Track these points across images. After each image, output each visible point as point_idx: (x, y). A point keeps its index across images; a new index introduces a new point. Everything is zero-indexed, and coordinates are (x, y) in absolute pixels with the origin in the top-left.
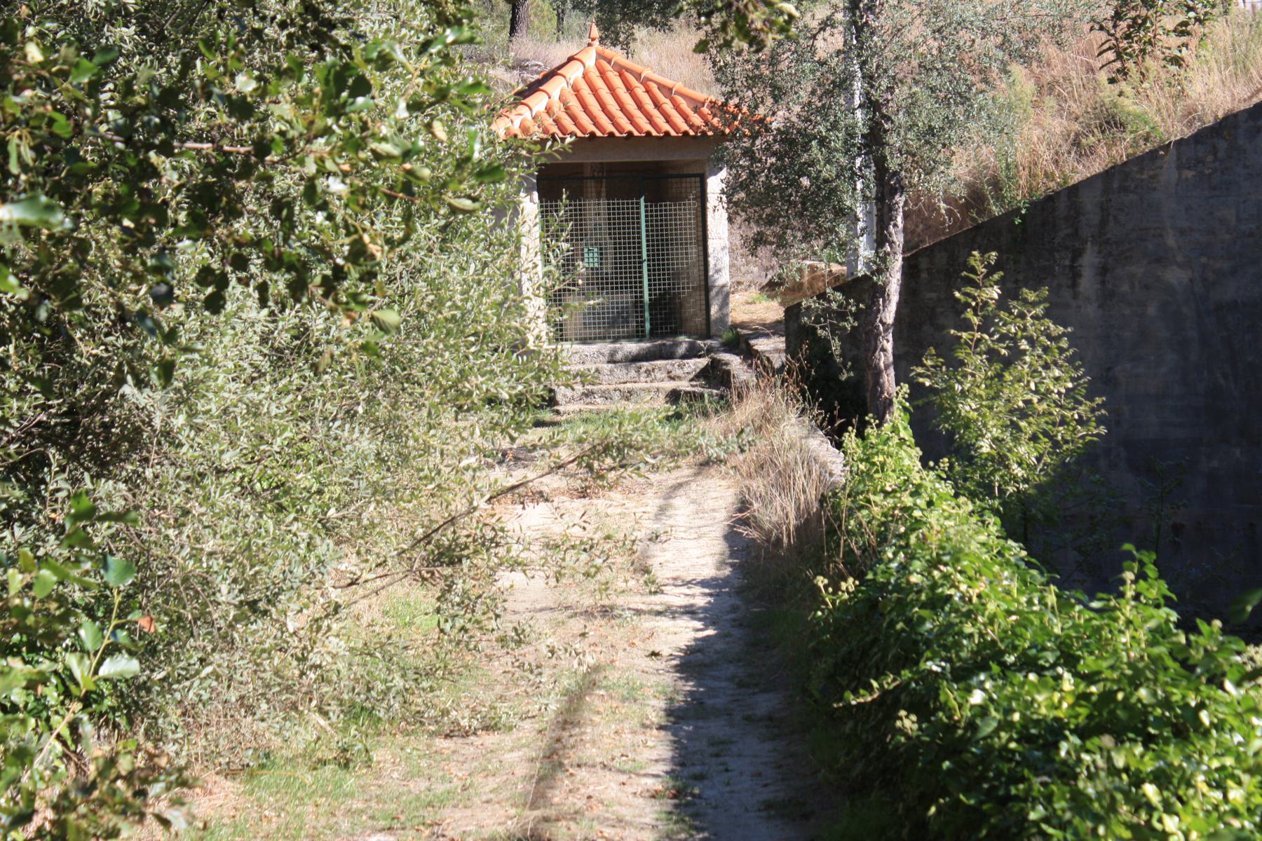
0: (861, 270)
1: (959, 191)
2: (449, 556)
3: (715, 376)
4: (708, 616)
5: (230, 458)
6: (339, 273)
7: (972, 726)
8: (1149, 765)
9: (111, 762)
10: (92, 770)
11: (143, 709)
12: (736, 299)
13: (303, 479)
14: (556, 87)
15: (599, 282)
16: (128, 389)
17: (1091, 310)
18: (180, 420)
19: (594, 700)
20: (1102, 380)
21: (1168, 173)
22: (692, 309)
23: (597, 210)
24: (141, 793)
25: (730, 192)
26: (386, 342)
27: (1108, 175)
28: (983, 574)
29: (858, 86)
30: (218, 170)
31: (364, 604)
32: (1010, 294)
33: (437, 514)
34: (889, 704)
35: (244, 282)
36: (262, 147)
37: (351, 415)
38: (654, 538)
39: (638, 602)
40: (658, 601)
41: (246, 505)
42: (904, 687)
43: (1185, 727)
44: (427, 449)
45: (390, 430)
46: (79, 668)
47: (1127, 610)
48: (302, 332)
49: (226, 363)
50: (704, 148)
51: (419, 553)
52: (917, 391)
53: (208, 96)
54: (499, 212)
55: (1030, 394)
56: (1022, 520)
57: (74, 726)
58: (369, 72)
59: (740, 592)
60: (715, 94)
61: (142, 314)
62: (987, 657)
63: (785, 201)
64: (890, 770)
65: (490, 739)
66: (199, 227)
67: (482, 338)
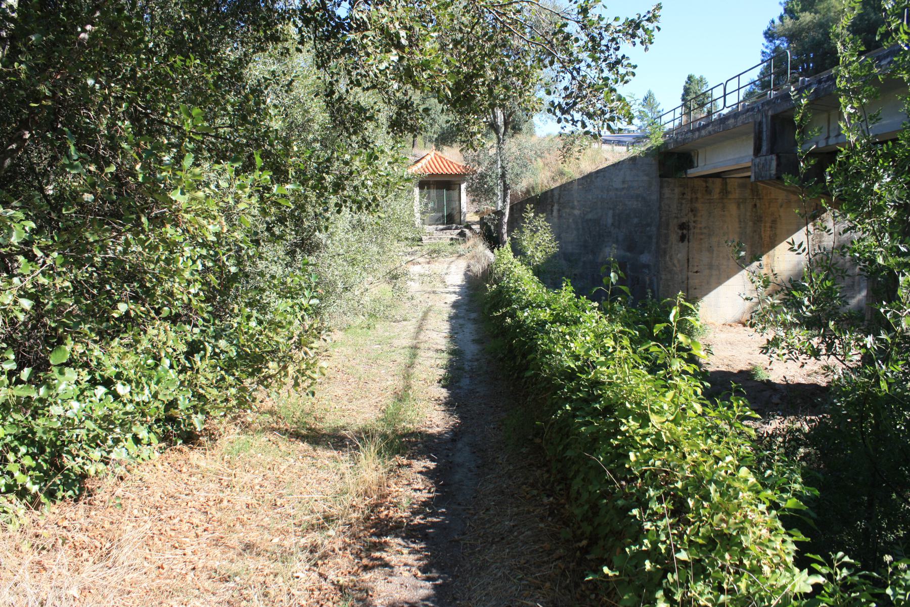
0: (499, 209)
1: (524, 190)
2: (395, 277)
3: (462, 234)
4: (460, 294)
5: (341, 252)
6: (370, 204)
7: (524, 321)
8: (567, 331)
9: (312, 325)
10: (307, 328)
11: (319, 313)
12: (467, 215)
13: (360, 258)
14: (423, 161)
15: (434, 210)
16: (317, 233)
17: (556, 220)
18: (329, 242)
19: (430, 314)
20: (558, 238)
21: (575, 187)
22: (456, 218)
23: (433, 192)
24: (319, 333)
25: (467, 188)
26: (380, 222)
27: (561, 186)
28: (530, 286)
29: (499, 163)
30: (340, 179)
31: (373, 289)
32: (536, 215)
33: (392, 267)
34: (504, 316)
35: (346, 207)
36: (351, 173)
37: (371, 241)
38: (446, 274)
39: (442, 290)
40: (447, 290)
41: (345, 263)
42: (507, 312)
43: (576, 322)
44: (390, 250)
45: (381, 245)
46: (304, 302)
47: (563, 294)
48: (359, 221)
49: (340, 228)
50: (461, 177)
51: (388, 276)
52: (512, 239)
53: (338, 160)
54: (409, 192)
55: (540, 240)
56: (538, 272)
57: (302, 317)
58: (378, 154)
59: (467, 288)
60: (464, 164)
61: (321, 214)
62: (529, 304)
63: (480, 191)
64: (503, 332)
65: (405, 323)
66: (335, 192)
67: (405, 223)
